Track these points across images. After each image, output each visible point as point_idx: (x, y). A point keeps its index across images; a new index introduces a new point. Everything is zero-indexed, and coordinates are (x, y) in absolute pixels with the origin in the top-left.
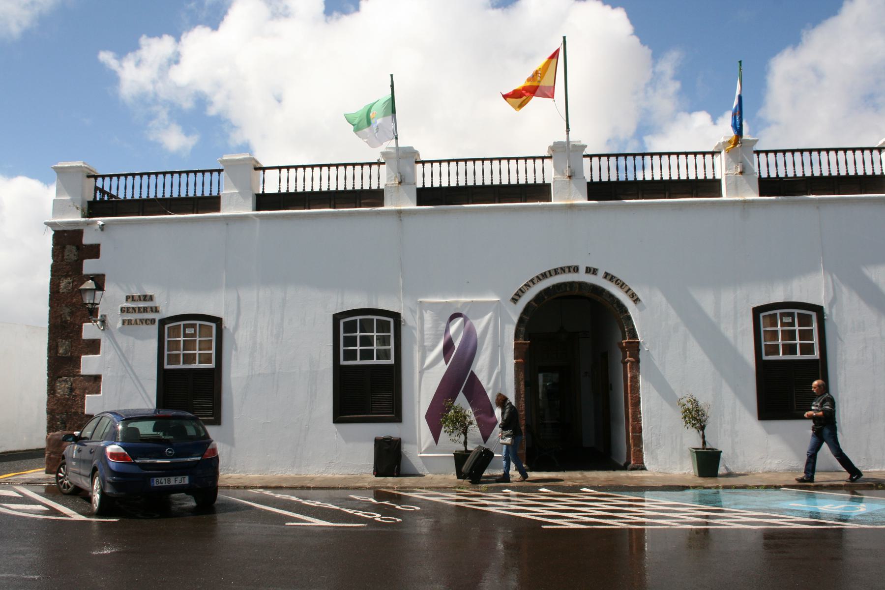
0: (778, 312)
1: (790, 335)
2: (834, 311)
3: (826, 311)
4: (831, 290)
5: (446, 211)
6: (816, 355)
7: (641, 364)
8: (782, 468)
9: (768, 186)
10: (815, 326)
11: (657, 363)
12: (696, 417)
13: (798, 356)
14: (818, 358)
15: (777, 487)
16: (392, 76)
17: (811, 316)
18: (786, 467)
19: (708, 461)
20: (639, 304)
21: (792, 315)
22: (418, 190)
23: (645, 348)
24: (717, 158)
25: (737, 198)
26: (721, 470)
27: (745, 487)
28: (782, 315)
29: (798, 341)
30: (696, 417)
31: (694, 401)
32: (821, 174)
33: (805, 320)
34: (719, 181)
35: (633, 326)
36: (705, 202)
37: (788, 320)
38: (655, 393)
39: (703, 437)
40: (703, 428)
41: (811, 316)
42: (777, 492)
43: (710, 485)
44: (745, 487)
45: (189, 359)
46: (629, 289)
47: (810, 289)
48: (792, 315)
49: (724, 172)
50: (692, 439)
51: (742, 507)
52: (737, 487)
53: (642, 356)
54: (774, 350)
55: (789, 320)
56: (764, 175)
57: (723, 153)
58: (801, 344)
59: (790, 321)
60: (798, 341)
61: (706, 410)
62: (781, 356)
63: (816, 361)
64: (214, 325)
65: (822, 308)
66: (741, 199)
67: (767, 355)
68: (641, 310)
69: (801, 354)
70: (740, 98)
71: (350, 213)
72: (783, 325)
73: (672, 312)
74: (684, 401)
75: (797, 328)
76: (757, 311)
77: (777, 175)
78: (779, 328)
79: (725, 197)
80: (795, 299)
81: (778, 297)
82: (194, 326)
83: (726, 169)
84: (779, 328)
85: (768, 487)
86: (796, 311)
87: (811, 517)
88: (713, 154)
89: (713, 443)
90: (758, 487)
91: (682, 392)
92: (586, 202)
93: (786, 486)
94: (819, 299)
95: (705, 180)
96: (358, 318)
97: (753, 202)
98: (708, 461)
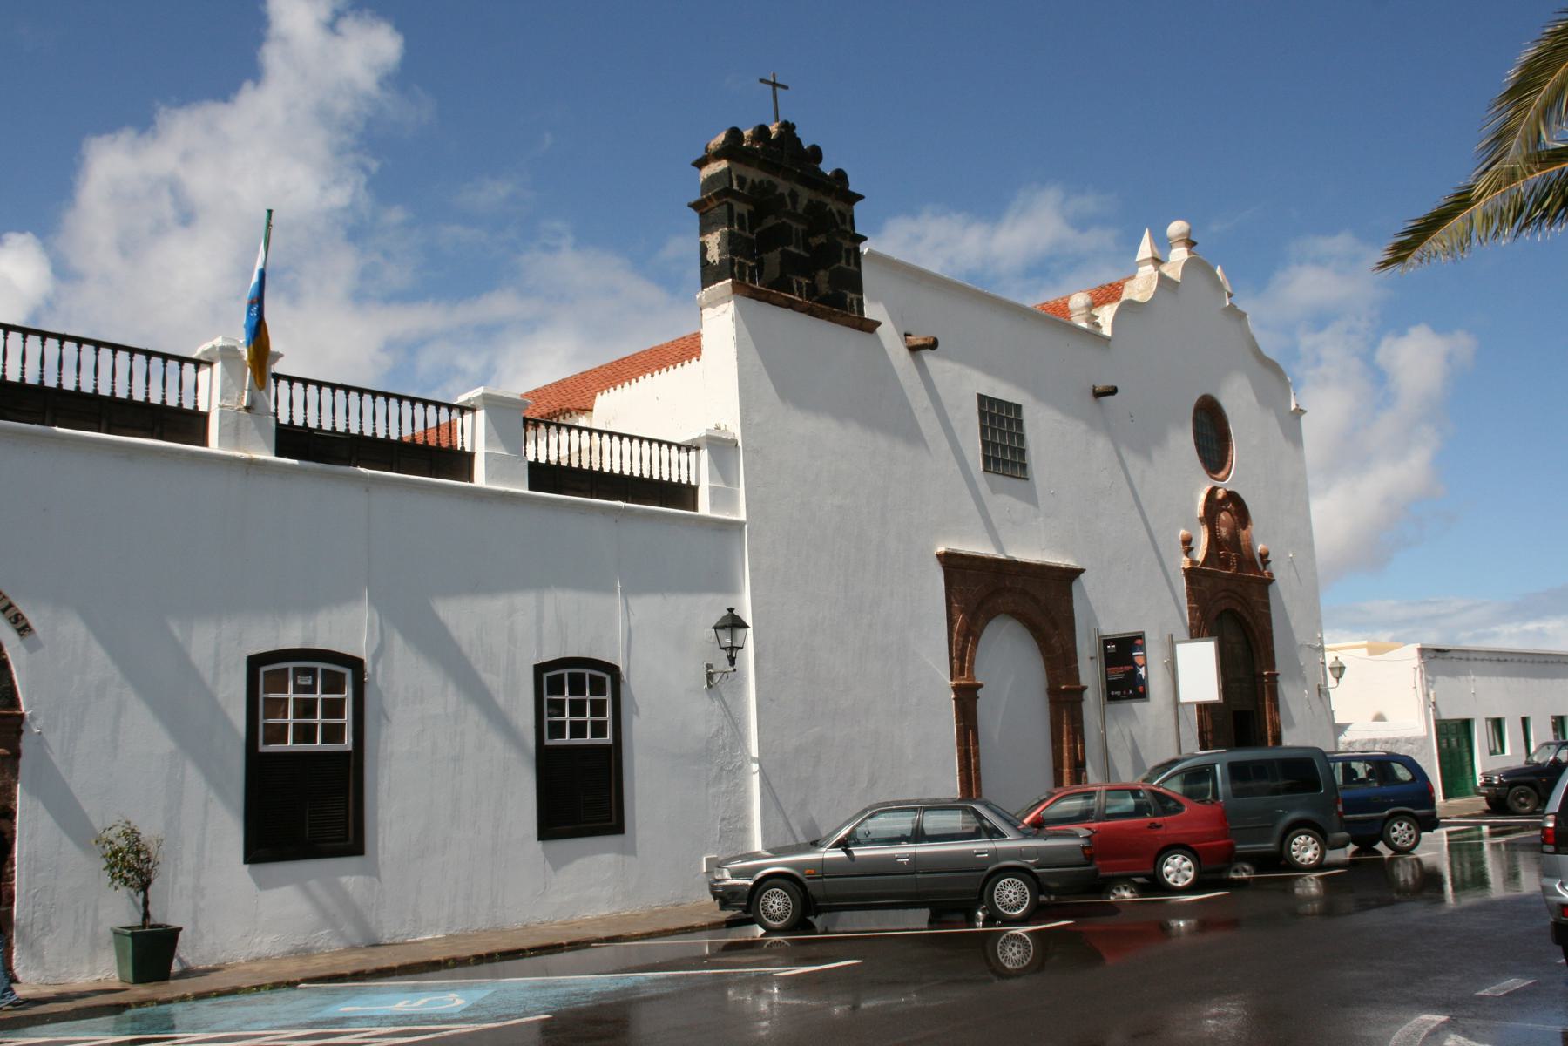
0: (291, 665)
1: (306, 708)
2: (379, 668)
3: (368, 668)
4: (377, 633)
5: (333, 475)
6: (347, 743)
7: (23, 762)
8: (282, 949)
9: (292, 440)
10: (348, 693)
11: (56, 758)
12: (132, 865)
13: (319, 745)
14: (350, 748)
15: (292, 985)
16: (270, 212)
17: (343, 675)
18: (287, 948)
19: (152, 951)
20: (29, 638)
21: (312, 672)
22: (530, 463)
23: (33, 728)
24: (204, 374)
25: (238, 454)
26: (176, 967)
27: (235, 991)
28: (297, 671)
29: (319, 719)
30: (132, 865)
31: (132, 835)
32: (130, 396)
33: (598, 686)
34: (205, 417)
35: (12, 681)
36: (179, 452)
37: (305, 681)
38: (46, 820)
39: (146, 903)
40: (145, 886)
41: (343, 675)
42: (292, 993)
43: (168, 996)
44: (235, 991)
45: (578, 730)
46: (11, 605)
47: (347, 629)
48: (312, 672)
49: (216, 401)
50: (120, 909)
51: (264, 1025)
52: (220, 994)
53: (26, 744)
54: (278, 734)
55: (308, 681)
56: (284, 420)
57: (218, 366)
58: (295, 725)
59: (310, 682)
60: (319, 719)
61: (152, 848)
62: (290, 746)
63: (346, 754)
64: (546, 675)
65: (362, 661)
66: (245, 455)
67: (266, 742)
68: (32, 648)
69: (324, 741)
70: (262, 274)
71: (22, 433)
72: (297, 689)
73: (98, 653)
74: (111, 835)
75: (319, 695)
76: (255, 662)
77: (23, 379)
78: (291, 695)
79: (214, 446)
80: (320, 644)
81: (292, 638)
82: (312, 672)
83: (222, 397)
84: (291, 695)
85: (276, 986)
86: (320, 666)
87: (395, 1025)
88: (198, 364)
89: (167, 912)
90: (258, 988)
91: (107, 817)
92: (271, 457)
93: (304, 981)
94: (360, 648)
95: (179, 410)
96: (566, 672)
97: (265, 463)
98: (152, 951)
